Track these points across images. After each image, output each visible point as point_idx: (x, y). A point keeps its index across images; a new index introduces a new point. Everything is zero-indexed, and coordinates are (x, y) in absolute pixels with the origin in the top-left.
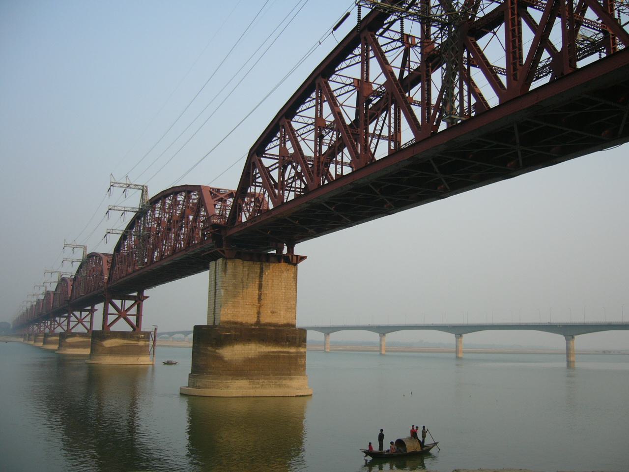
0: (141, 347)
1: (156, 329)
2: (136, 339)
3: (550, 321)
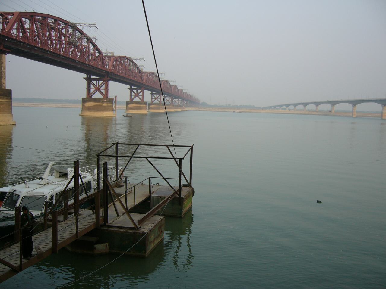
0: (105, 107)
1: (116, 97)
2: (101, 102)
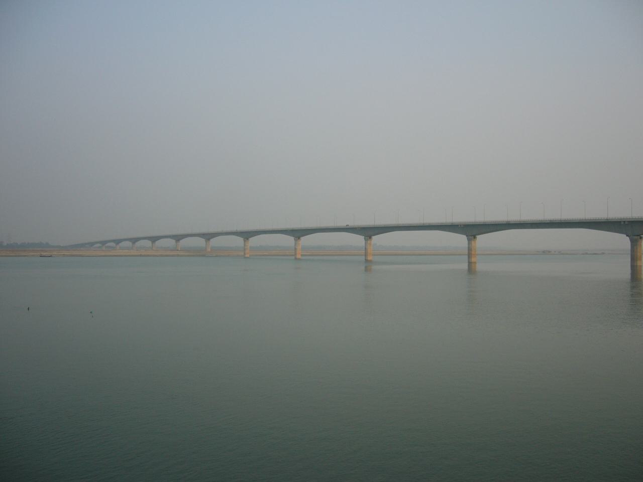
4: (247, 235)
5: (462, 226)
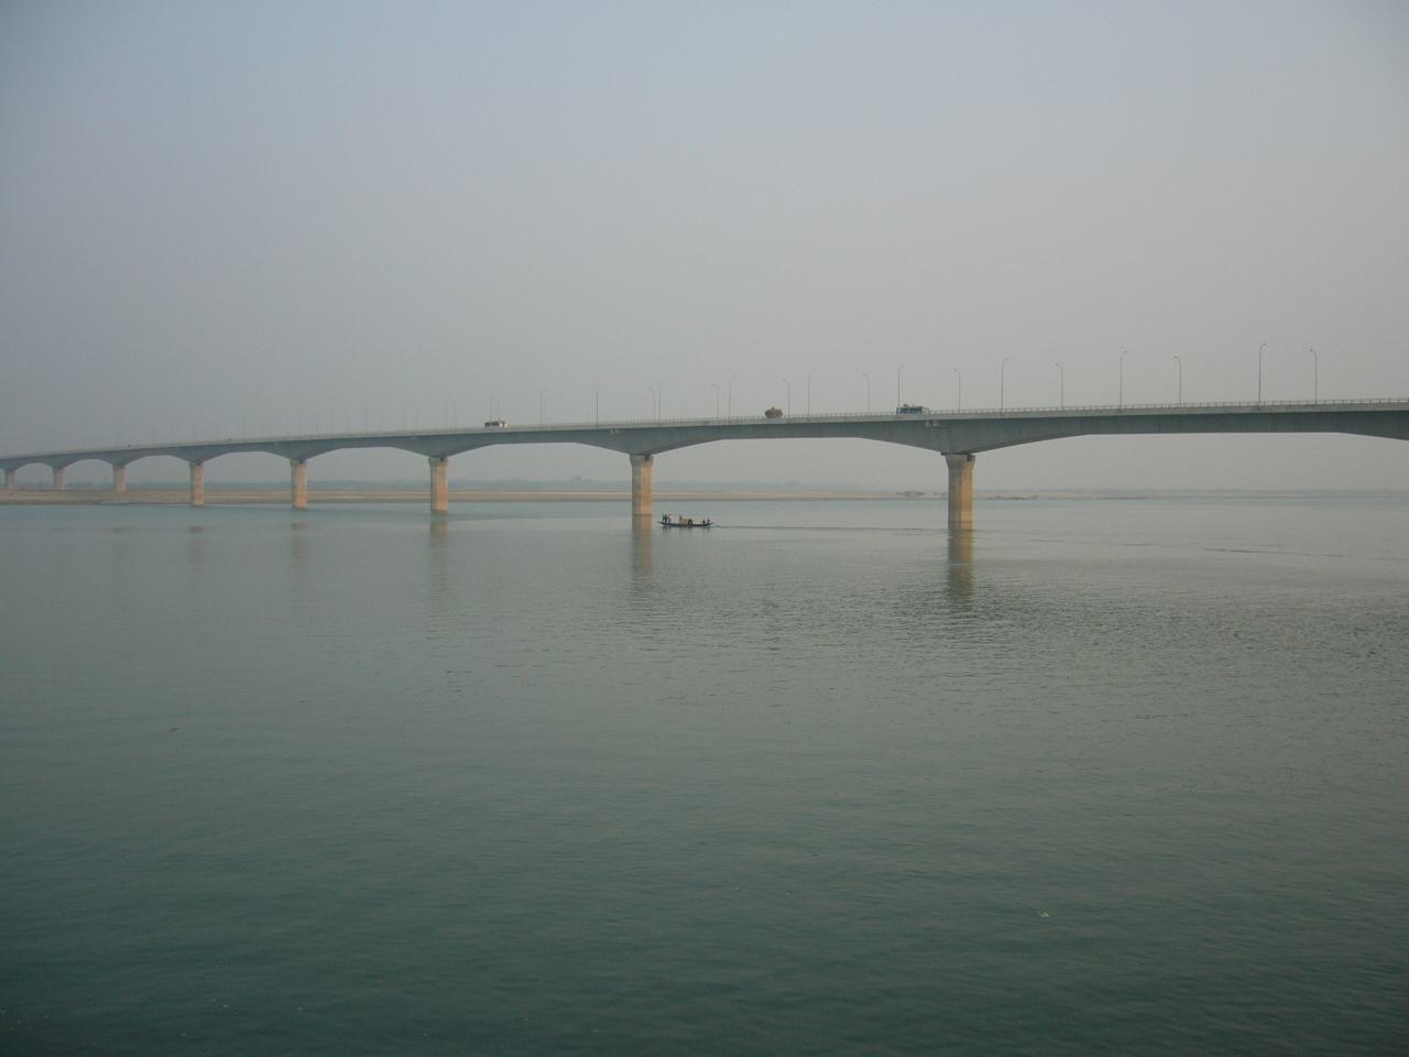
3: (657, 418)
4: (300, 450)
5: (935, 425)
